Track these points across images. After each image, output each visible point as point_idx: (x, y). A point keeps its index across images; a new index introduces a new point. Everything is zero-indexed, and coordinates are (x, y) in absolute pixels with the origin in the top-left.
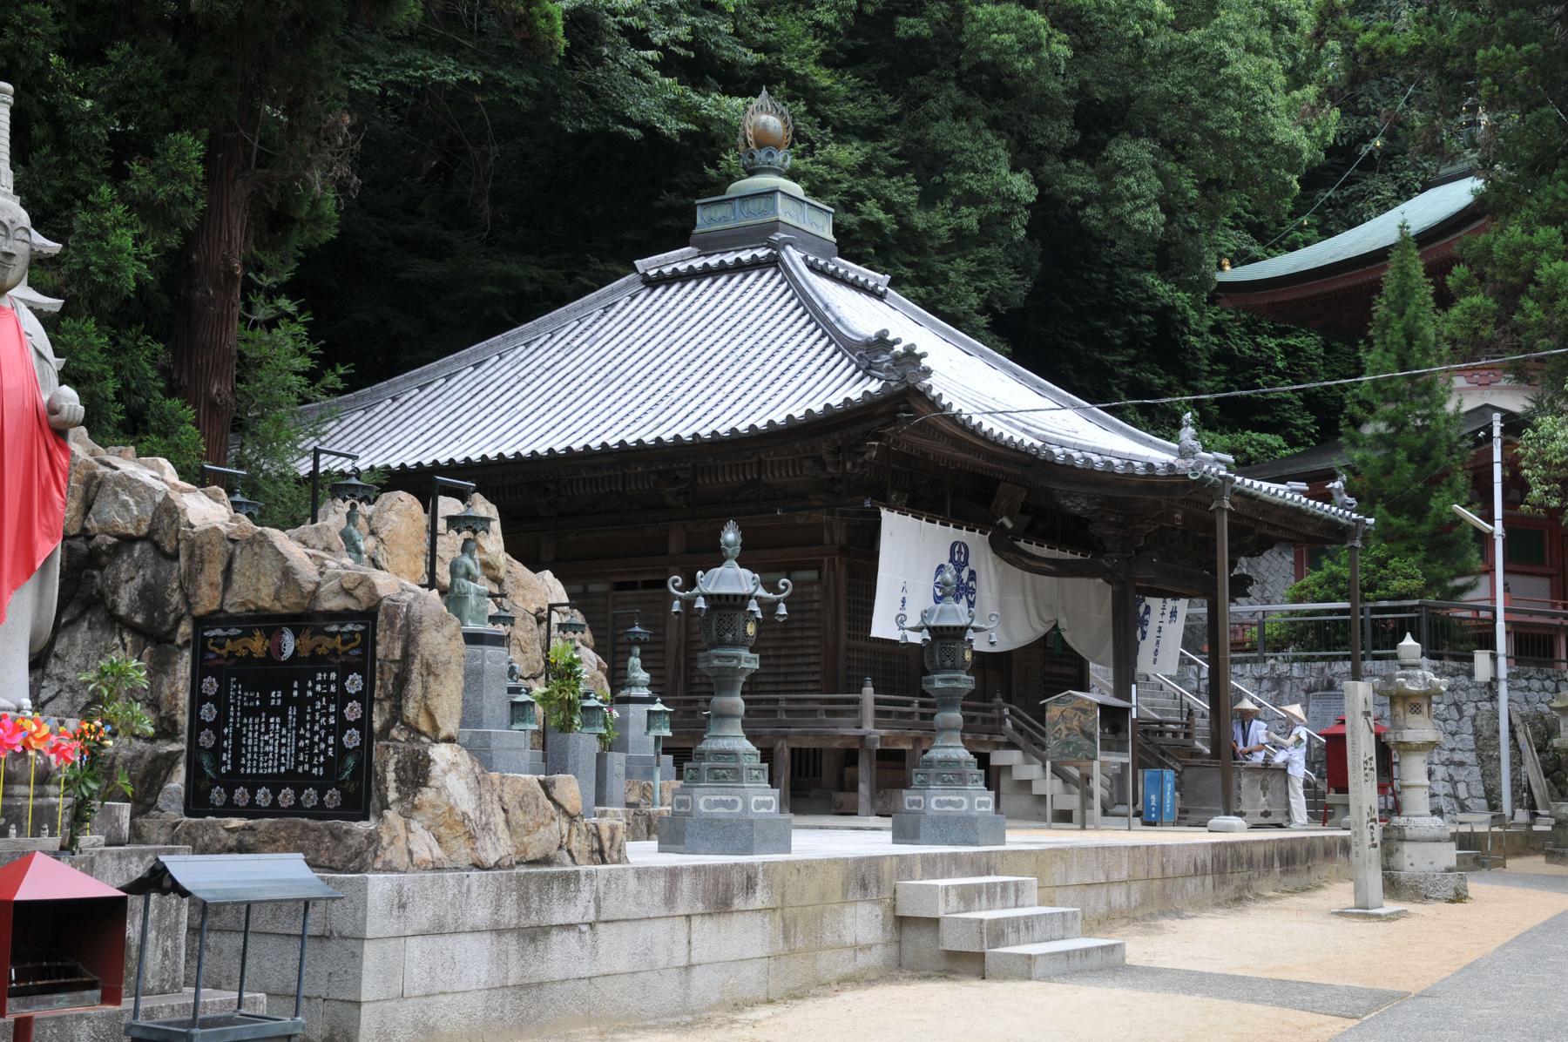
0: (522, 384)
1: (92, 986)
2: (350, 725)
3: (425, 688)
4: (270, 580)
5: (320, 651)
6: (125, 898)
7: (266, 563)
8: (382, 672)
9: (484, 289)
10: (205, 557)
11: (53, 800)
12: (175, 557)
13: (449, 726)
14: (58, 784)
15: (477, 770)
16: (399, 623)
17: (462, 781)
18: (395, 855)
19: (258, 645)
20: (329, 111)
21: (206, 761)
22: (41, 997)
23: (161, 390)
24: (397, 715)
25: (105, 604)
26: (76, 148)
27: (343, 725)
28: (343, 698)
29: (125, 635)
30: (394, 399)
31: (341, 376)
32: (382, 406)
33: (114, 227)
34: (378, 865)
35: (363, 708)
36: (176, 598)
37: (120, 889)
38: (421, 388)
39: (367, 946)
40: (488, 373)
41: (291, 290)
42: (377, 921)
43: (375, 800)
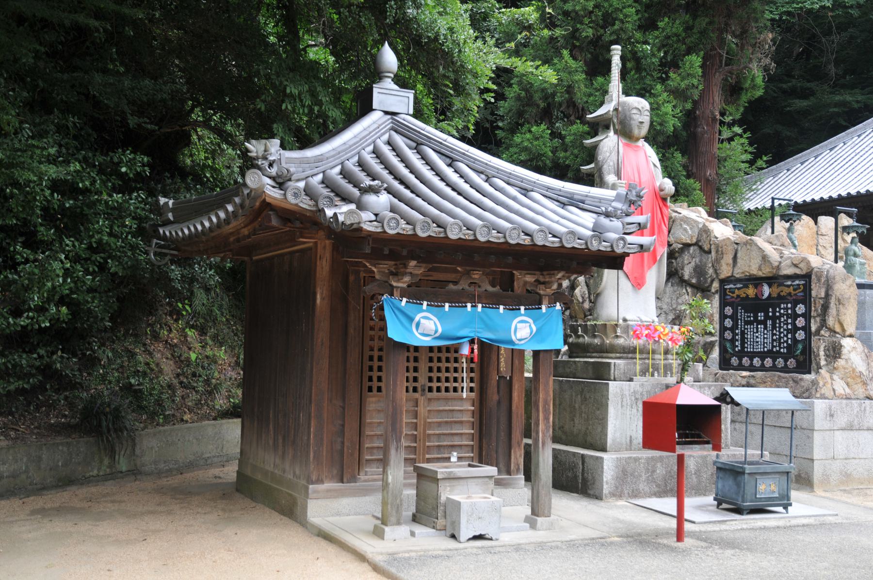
0: (858, 156)
1: (707, 443)
2: (799, 329)
3: (838, 311)
4: (756, 262)
5: (782, 294)
6: (719, 406)
7: (754, 253)
8: (815, 304)
9: (831, 110)
10: (724, 252)
11: (671, 361)
12: (709, 252)
13: (851, 329)
14: (673, 354)
15: (866, 351)
16: (823, 280)
17: (859, 356)
18: (826, 391)
19: (751, 292)
20: (760, 33)
21: (728, 345)
22: (688, 446)
23: (684, 176)
24: (823, 324)
25: (678, 275)
26: (645, 70)
27: (796, 329)
28: (795, 316)
29: (688, 288)
30: (788, 170)
31: (764, 161)
32: (782, 174)
33: (663, 104)
34: (818, 395)
35: (806, 320)
36: (711, 271)
37: (716, 399)
38: (802, 164)
39: (815, 433)
40: (838, 152)
41: (740, 123)
42: (820, 422)
43: (814, 365)
